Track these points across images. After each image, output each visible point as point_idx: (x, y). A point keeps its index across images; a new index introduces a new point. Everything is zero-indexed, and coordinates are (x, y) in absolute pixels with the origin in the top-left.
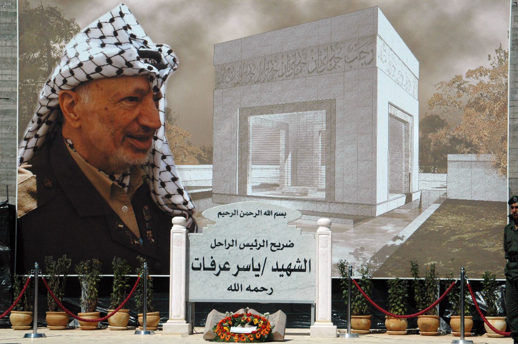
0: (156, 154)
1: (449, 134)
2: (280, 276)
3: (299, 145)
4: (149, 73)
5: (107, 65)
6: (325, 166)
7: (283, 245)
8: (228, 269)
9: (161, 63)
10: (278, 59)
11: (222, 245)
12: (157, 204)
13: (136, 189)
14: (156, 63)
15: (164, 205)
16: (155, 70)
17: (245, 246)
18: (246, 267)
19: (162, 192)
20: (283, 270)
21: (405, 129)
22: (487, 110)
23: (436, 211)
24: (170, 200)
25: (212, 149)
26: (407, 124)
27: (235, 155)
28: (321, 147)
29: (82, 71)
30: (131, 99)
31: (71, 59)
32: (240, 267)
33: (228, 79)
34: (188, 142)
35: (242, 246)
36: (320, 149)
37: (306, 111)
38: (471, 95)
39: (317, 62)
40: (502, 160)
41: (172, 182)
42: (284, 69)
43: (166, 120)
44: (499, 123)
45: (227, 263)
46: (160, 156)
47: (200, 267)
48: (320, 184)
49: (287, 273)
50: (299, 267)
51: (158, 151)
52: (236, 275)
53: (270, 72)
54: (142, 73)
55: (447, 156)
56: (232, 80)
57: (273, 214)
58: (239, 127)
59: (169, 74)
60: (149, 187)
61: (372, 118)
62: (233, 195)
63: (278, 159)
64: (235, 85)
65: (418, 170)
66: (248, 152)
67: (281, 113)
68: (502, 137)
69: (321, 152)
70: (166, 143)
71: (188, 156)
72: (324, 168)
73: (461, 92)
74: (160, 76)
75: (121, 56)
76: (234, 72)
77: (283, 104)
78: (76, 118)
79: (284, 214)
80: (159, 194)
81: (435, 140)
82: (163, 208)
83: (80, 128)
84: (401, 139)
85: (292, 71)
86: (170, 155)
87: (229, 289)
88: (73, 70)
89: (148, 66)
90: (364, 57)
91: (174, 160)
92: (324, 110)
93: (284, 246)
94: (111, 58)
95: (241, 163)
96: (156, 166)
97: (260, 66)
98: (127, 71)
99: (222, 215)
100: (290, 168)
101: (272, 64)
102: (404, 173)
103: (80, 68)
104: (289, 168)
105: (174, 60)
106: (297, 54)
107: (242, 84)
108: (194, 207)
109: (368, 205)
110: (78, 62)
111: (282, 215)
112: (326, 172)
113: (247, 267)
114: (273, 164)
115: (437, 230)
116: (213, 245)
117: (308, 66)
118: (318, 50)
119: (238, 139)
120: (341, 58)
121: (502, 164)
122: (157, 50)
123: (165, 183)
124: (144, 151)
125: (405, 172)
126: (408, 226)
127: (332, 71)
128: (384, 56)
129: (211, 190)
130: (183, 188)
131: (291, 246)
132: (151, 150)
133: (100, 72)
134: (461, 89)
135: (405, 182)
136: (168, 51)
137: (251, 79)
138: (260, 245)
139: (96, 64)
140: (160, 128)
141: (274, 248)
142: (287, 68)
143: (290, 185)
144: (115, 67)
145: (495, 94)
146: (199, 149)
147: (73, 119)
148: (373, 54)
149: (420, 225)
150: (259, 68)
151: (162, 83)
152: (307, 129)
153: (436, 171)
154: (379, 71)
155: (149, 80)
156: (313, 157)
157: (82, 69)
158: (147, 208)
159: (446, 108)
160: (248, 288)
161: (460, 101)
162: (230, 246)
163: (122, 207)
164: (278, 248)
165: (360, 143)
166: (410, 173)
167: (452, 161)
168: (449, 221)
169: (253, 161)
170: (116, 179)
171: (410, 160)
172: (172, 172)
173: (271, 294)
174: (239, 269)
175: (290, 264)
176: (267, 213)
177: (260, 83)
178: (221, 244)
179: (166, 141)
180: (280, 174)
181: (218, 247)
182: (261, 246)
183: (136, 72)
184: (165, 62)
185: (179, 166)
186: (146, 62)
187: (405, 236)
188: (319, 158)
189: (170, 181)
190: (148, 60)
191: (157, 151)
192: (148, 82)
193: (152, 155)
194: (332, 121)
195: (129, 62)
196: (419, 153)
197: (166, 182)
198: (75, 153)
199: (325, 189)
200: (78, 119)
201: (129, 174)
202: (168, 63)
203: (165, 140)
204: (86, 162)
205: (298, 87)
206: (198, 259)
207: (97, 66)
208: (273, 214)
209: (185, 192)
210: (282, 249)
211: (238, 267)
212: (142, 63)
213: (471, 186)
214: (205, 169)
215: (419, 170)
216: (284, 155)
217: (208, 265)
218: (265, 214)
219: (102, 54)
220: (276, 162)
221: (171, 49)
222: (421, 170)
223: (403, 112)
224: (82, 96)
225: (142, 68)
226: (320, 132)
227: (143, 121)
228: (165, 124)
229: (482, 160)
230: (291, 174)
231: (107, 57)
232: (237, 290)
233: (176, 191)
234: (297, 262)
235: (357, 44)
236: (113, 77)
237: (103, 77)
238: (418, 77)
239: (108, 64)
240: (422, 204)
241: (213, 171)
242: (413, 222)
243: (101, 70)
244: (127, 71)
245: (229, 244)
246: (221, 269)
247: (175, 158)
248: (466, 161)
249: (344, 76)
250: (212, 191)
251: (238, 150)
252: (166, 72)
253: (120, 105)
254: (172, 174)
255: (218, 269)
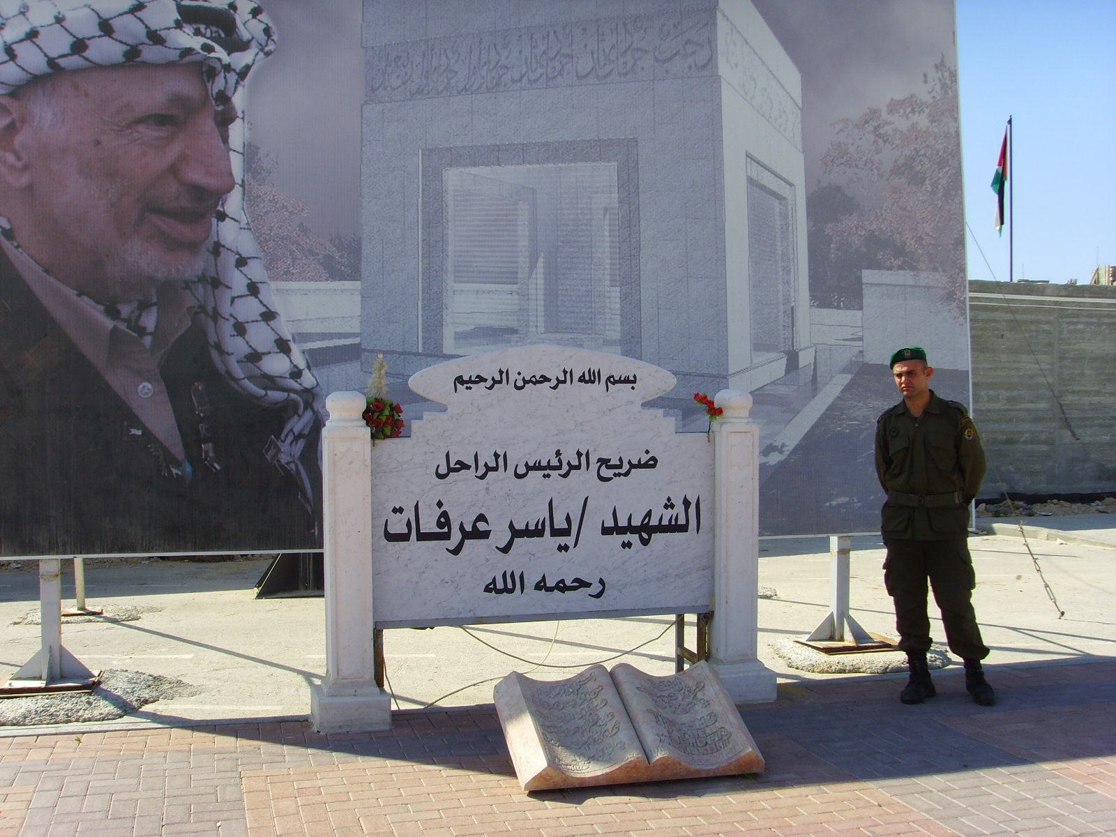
0: (222, 255)
1: (863, 228)
2: (624, 545)
3: (562, 239)
4: (205, 59)
5: (99, 37)
6: (618, 289)
7: (630, 462)
8: (485, 535)
9: (235, 36)
10: (509, 43)
11: (468, 467)
12: (226, 376)
13: (173, 340)
14: (223, 35)
15: (244, 379)
16: (220, 53)
17: (529, 468)
18: (532, 527)
19: (237, 346)
20: (630, 529)
21: (780, 213)
22: (927, 182)
23: (843, 391)
24: (259, 368)
25: (359, 242)
26: (784, 202)
27: (415, 258)
28: (608, 244)
29: (37, 48)
30: (161, 120)
31: (9, 18)
32: (517, 527)
33: (396, 82)
34: (301, 225)
35: (522, 470)
36: (607, 250)
37: (575, 163)
38: (898, 149)
39: (595, 56)
40: (956, 285)
41: (262, 322)
42: (524, 66)
43: (247, 172)
44: (949, 211)
45: (482, 518)
46: (233, 259)
47: (406, 531)
48: (608, 327)
49: (641, 538)
50: (670, 520)
51: (227, 247)
52: (506, 550)
53: (493, 69)
54: (188, 59)
55: (861, 273)
56: (404, 83)
57: (603, 379)
58: (423, 194)
59: (253, 63)
60: (204, 333)
61: (714, 185)
62: (409, 354)
63: (515, 270)
64: (412, 95)
65: (808, 300)
66: (444, 251)
67: (518, 164)
68: (956, 238)
69: (610, 256)
70: (246, 226)
71: (301, 259)
72: (615, 293)
73: (880, 142)
74: (233, 67)
75: (135, 16)
76: (409, 66)
77: (523, 144)
78: (19, 164)
79: (631, 378)
80: (230, 352)
81: (838, 238)
82: (241, 387)
83: (30, 189)
84: (773, 233)
85: (542, 71)
86: (257, 258)
87: (487, 589)
88: (14, 47)
89: (201, 43)
90: (694, 53)
91: (268, 269)
92: (614, 161)
93: (632, 466)
94: (111, 22)
95: (429, 278)
96: (221, 283)
97: (470, 55)
98: (150, 53)
99: (465, 385)
100: (541, 292)
101: (498, 53)
102: (781, 307)
103: (32, 41)
104: (538, 291)
105: (267, 31)
106: (552, 34)
107: (428, 93)
108: (318, 384)
109: (712, 376)
110: (27, 28)
111: (627, 381)
112: (622, 301)
113: (537, 525)
114: (504, 280)
115: (847, 431)
116: (443, 470)
117: (577, 63)
118: (598, 30)
119: (420, 220)
120: (646, 52)
121: (958, 294)
122: (226, 7)
123: (246, 325)
124: (192, 247)
125: (784, 304)
126: (793, 421)
127: (628, 76)
128: (733, 53)
129: (357, 343)
130: (290, 337)
131: (652, 463)
132: (209, 244)
133: (84, 54)
134: (880, 136)
135: (784, 326)
136: (252, 10)
137: (449, 83)
138: (569, 463)
139: (71, 34)
140: (233, 191)
141: (605, 472)
142: (531, 63)
143: (541, 329)
144: (121, 42)
145: (938, 151)
146: (328, 243)
147: (12, 168)
148: (711, 47)
149: (815, 420)
150: (468, 60)
151: (237, 83)
152: (577, 203)
153: (842, 303)
154: (723, 83)
155: (205, 75)
156: (593, 267)
157: (38, 46)
158: (200, 388)
159: (856, 174)
160: (540, 582)
161: (880, 160)
162: (489, 469)
163: (138, 385)
164: (617, 471)
165: (691, 238)
166: (792, 308)
167: (871, 284)
168: (869, 411)
169: (457, 274)
170: (122, 317)
171: (792, 280)
172: (262, 299)
173: (599, 595)
174: (516, 533)
175: (649, 514)
176: (587, 378)
177: (469, 92)
178: (463, 466)
179: (248, 224)
180: (519, 304)
181: (456, 473)
182: (571, 467)
183: (174, 56)
184: (246, 36)
185: (279, 283)
186: (197, 33)
187: (787, 444)
188: (605, 269)
189: (257, 321)
190: (202, 28)
191: (224, 246)
192: (203, 80)
193: (212, 258)
194: (631, 186)
195: (156, 31)
196: (809, 266)
197: (247, 322)
198: (16, 251)
199: (620, 340)
200: (26, 168)
201: (155, 304)
202: (253, 38)
203: (244, 221)
204: (44, 274)
205: (555, 108)
206: (401, 510)
207: (75, 39)
208: (603, 379)
209: (293, 346)
210: (626, 474)
211: (511, 526)
212: (189, 35)
213: (906, 337)
214: (342, 291)
215: (811, 301)
216: (528, 260)
217: (429, 525)
218: (582, 379)
219: (87, 11)
220: (510, 277)
221: (259, 6)
222: (815, 302)
223: (775, 175)
224: (35, 111)
225: (188, 46)
226: (606, 210)
227: (190, 175)
228: (243, 181)
229: (923, 284)
230: (544, 306)
231: (100, 17)
232: (511, 591)
233: (273, 343)
234: (666, 507)
235: (678, 24)
236: (113, 67)
237: (90, 65)
238: (800, 105)
239: (102, 34)
240: (818, 374)
241: (363, 297)
242: (801, 413)
243: (85, 47)
244: (150, 53)
245: (486, 465)
246: (466, 535)
247: (270, 265)
248: (896, 286)
249: (653, 89)
250: (359, 344)
251: (420, 248)
252: (241, 59)
253: (132, 133)
254: (261, 302)
255: (456, 536)
